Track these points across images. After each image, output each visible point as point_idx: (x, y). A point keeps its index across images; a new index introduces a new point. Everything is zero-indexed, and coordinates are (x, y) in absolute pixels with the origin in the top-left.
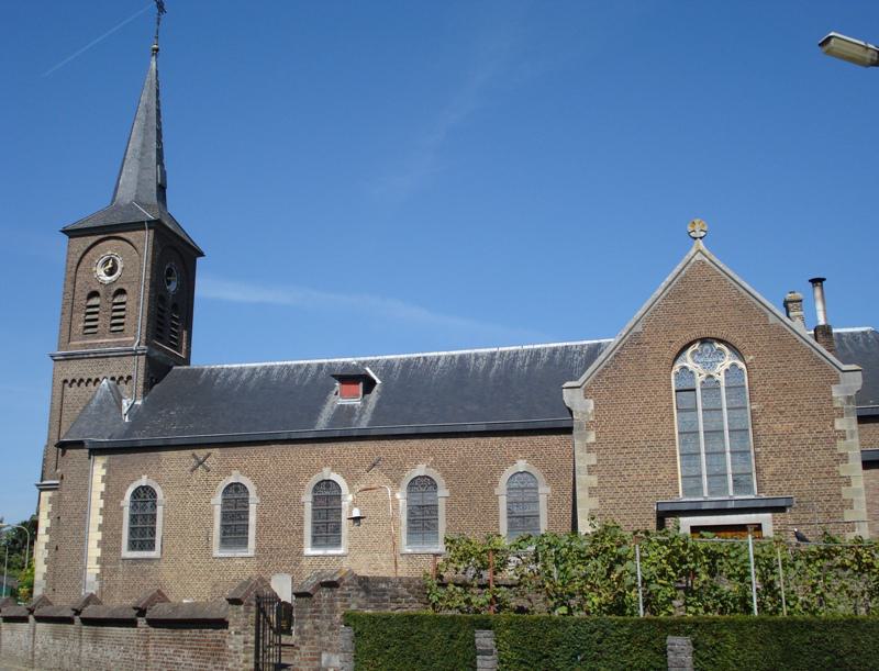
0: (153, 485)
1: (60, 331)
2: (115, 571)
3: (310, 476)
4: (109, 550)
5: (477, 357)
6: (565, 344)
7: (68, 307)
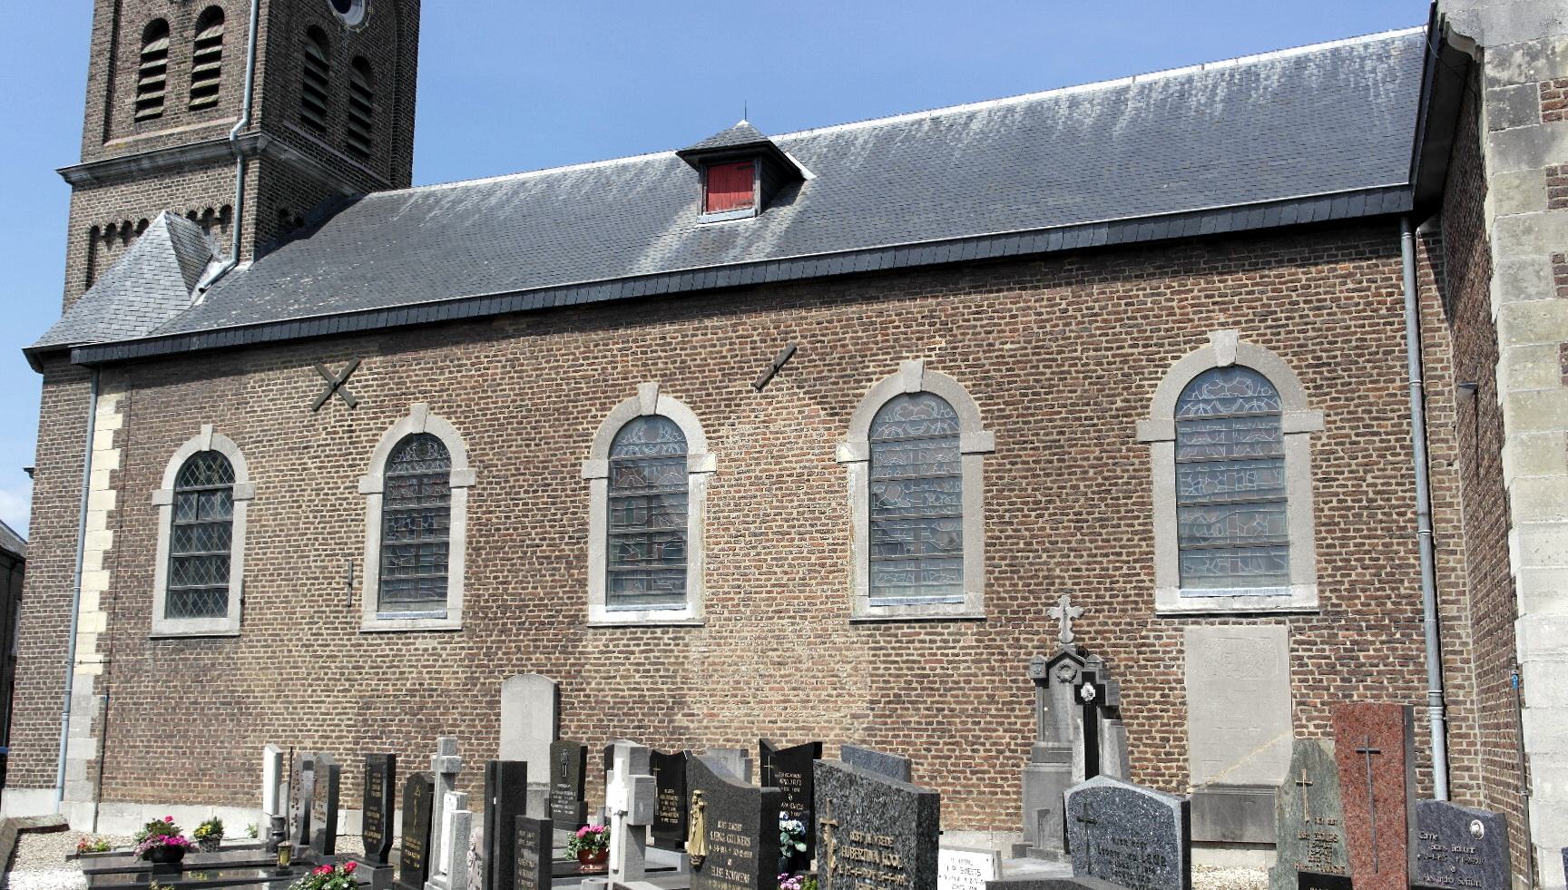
1: (87, 116)
2: (136, 670)
3: (603, 407)
4: (128, 614)
5: (1074, 102)
6: (1329, 46)
7: (104, 62)
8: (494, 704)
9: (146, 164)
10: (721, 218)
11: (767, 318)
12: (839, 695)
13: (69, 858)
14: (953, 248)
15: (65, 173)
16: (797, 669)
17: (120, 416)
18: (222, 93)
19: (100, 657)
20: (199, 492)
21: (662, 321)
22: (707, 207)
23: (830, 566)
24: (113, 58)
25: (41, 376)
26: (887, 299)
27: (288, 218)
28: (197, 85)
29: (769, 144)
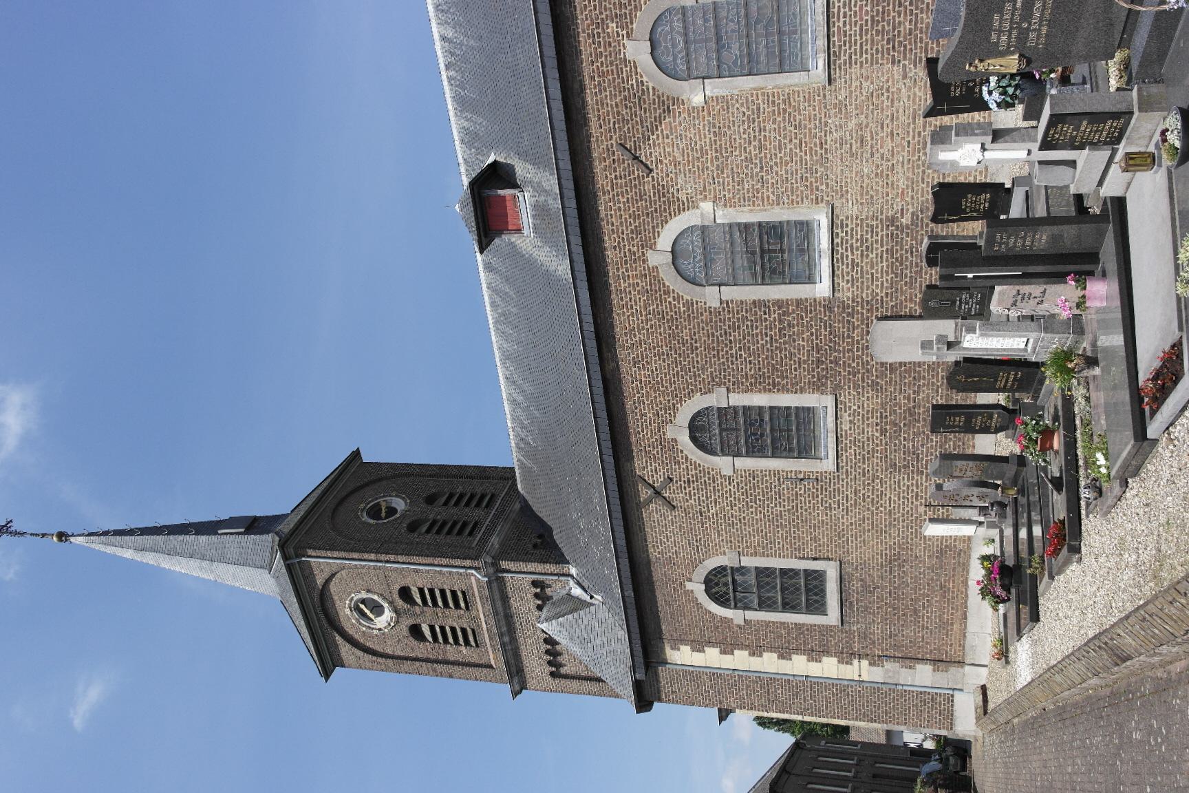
0: (701, 572)
2: (864, 636)
3: (667, 292)
7: (439, 667)
8: (893, 367)
9: (506, 639)
10: (526, 218)
11: (598, 168)
12: (888, 90)
13: (1007, 662)
14: (544, 42)
15: (515, 694)
16: (867, 126)
17: (683, 647)
18: (456, 588)
19: (855, 662)
20: (735, 591)
21: (604, 250)
22: (519, 230)
23: (784, 105)
24: (437, 661)
25: (656, 704)
26: (580, 74)
27: (539, 542)
28: (451, 605)
29: (472, 184)
